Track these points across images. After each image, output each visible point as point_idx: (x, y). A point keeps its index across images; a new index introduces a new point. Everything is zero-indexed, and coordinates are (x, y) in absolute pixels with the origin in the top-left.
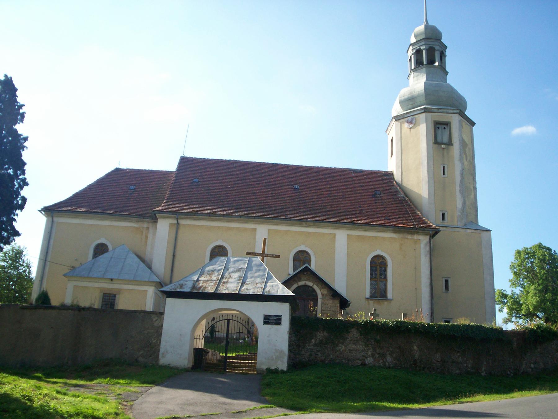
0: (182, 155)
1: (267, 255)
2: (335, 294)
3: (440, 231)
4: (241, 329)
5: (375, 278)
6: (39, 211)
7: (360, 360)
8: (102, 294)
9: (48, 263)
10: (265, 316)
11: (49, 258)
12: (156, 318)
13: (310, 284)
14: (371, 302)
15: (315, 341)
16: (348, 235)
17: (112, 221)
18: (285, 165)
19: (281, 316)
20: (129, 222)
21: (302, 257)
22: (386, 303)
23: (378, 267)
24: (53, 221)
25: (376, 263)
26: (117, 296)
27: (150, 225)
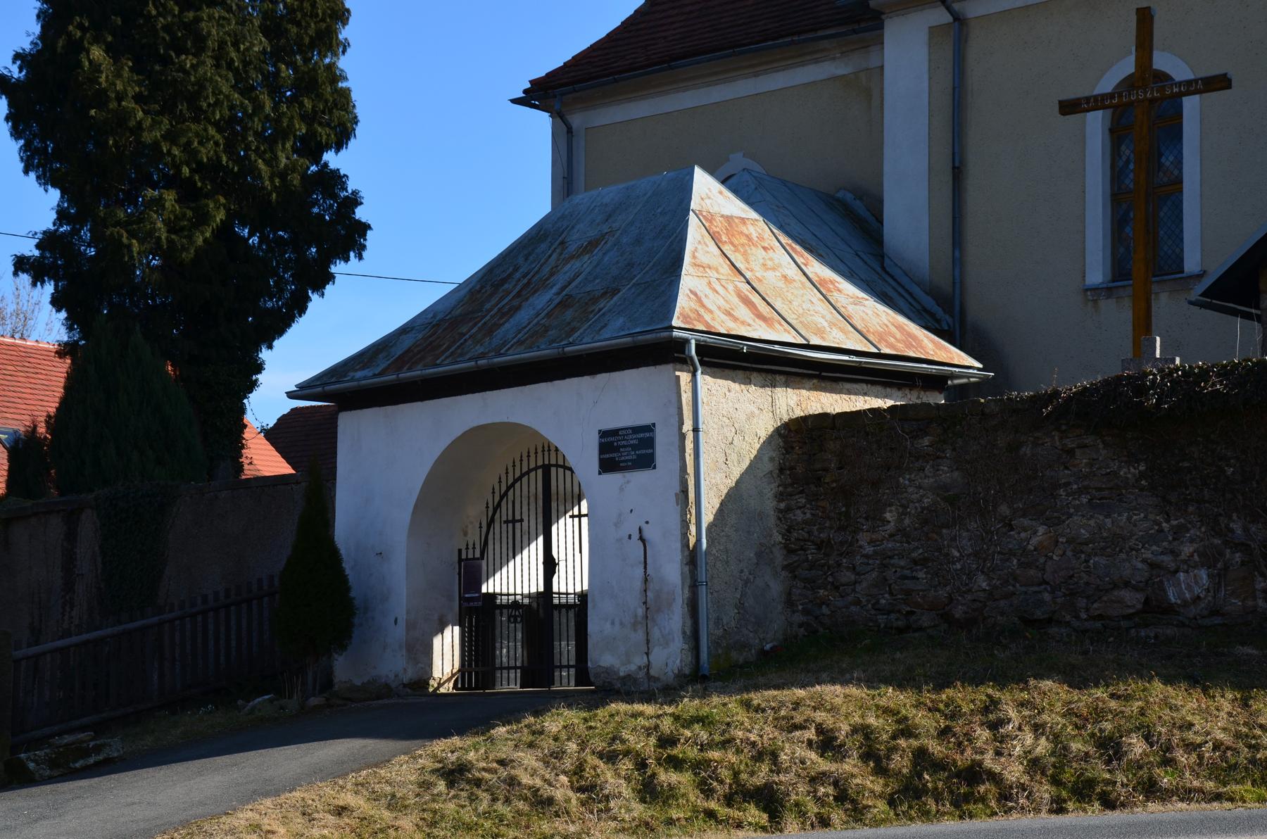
7: (1136, 589)
10: (604, 434)
15: (900, 520)
17: (756, 75)
20: (816, 61)
24: (570, 131)
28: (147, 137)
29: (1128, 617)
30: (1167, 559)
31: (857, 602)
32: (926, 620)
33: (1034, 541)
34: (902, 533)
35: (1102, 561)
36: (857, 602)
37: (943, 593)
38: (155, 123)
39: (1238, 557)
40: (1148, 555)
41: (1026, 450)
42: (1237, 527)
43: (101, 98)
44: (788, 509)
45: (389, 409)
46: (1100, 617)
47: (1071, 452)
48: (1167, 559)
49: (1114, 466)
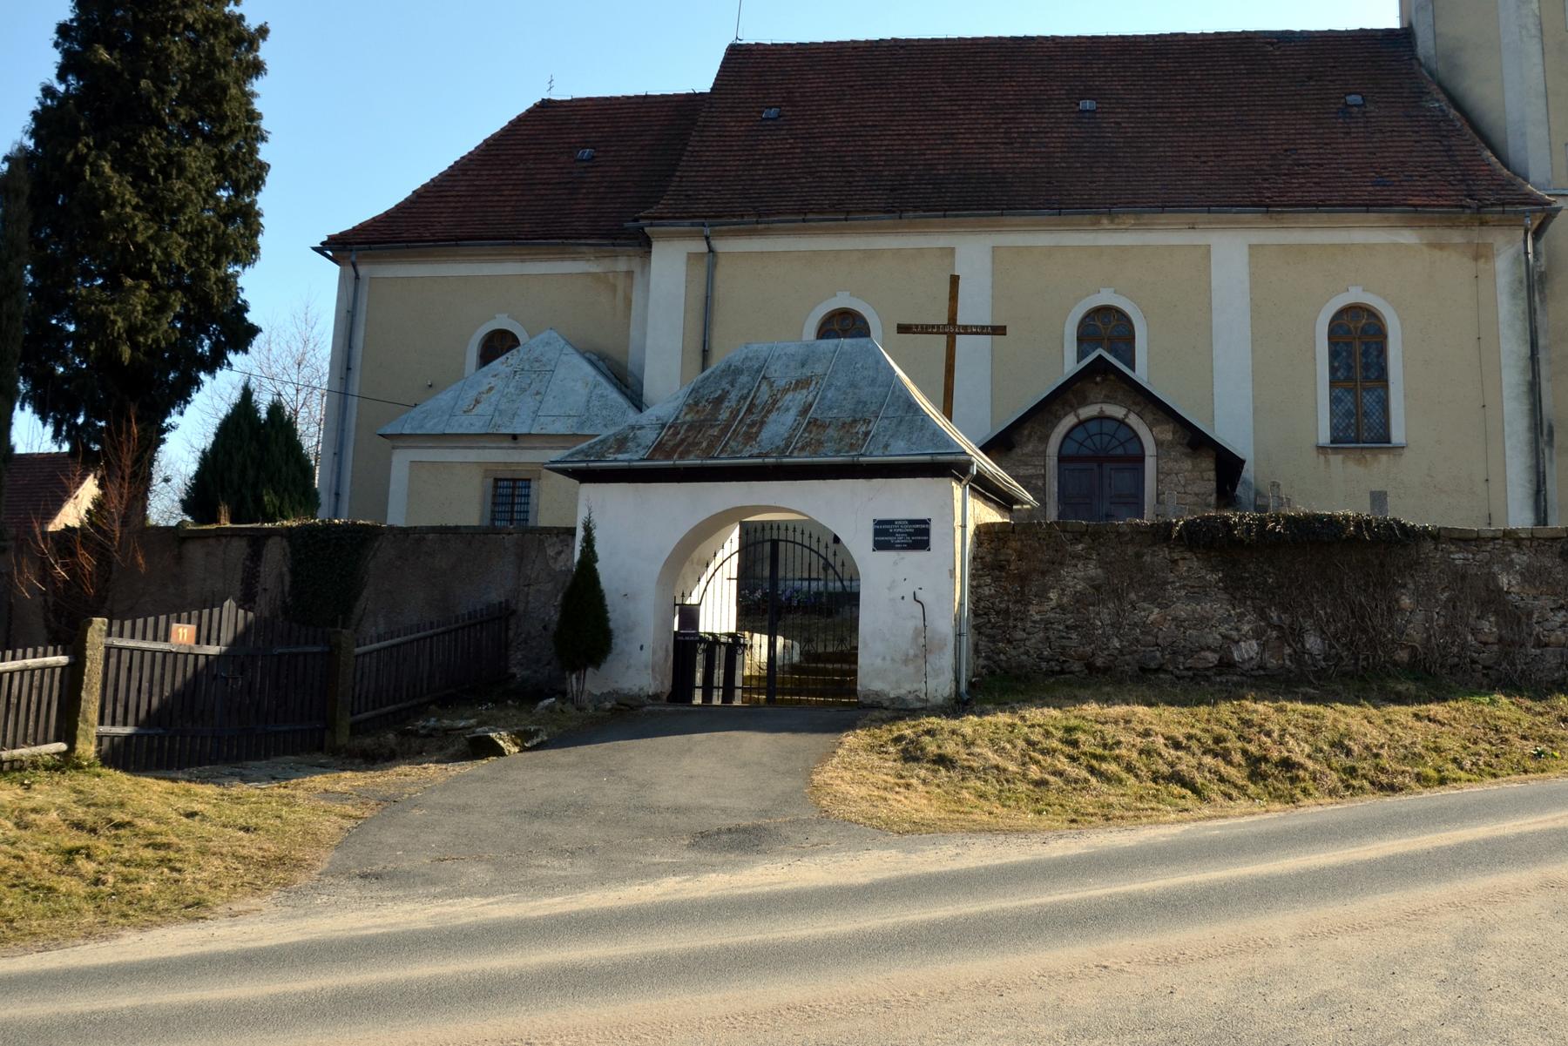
0: (730, 40)
1: (965, 327)
2: (1197, 441)
3: (1559, 210)
4: (814, 567)
5: (1348, 379)
6: (315, 249)
7: (1214, 651)
8: (491, 481)
9: (353, 402)
10: (878, 523)
11: (355, 388)
12: (558, 548)
13: (1117, 411)
14: (1336, 459)
15: (1060, 598)
16: (1250, 246)
17: (523, 261)
18: (1054, 38)
19: (926, 522)
20: (574, 259)
21: (1106, 329)
22: (1384, 458)
23: (1358, 345)
24: (357, 277)
25: (1349, 330)
26: (533, 484)
27: (635, 265)
28: (140, 239)
29: (1208, 669)
30: (1234, 633)
31: (1027, 653)
32: (1076, 667)
33: (1152, 617)
34: (1061, 608)
35: (1195, 633)
36: (1027, 653)
37: (1088, 649)
38: (147, 228)
39: (1275, 634)
40: (1222, 630)
41: (1147, 558)
42: (1274, 615)
43: (109, 201)
44: (979, 586)
45: (641, 485)
46: (1188, 669)
47: (1175, 562)
48: (1234, 633)
49: (1203, 572)
